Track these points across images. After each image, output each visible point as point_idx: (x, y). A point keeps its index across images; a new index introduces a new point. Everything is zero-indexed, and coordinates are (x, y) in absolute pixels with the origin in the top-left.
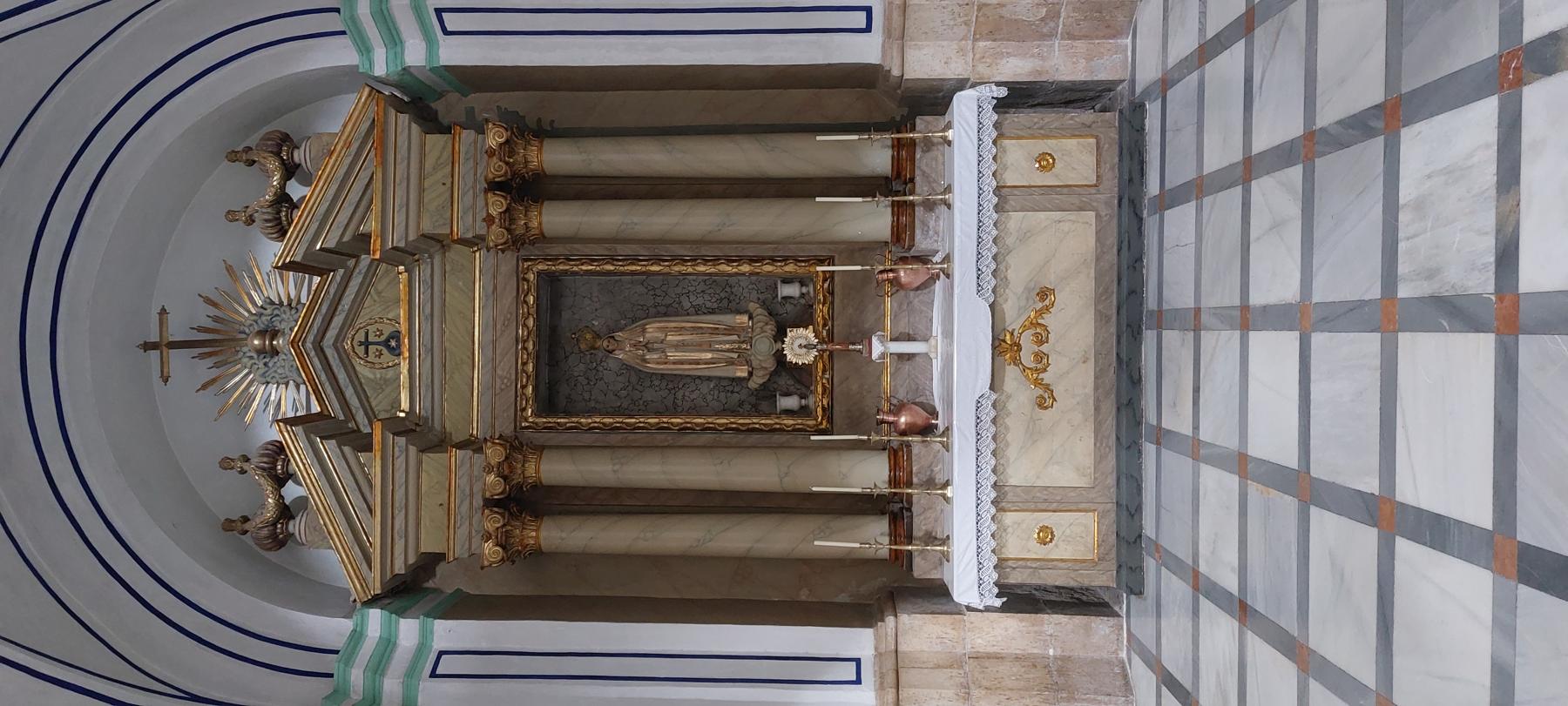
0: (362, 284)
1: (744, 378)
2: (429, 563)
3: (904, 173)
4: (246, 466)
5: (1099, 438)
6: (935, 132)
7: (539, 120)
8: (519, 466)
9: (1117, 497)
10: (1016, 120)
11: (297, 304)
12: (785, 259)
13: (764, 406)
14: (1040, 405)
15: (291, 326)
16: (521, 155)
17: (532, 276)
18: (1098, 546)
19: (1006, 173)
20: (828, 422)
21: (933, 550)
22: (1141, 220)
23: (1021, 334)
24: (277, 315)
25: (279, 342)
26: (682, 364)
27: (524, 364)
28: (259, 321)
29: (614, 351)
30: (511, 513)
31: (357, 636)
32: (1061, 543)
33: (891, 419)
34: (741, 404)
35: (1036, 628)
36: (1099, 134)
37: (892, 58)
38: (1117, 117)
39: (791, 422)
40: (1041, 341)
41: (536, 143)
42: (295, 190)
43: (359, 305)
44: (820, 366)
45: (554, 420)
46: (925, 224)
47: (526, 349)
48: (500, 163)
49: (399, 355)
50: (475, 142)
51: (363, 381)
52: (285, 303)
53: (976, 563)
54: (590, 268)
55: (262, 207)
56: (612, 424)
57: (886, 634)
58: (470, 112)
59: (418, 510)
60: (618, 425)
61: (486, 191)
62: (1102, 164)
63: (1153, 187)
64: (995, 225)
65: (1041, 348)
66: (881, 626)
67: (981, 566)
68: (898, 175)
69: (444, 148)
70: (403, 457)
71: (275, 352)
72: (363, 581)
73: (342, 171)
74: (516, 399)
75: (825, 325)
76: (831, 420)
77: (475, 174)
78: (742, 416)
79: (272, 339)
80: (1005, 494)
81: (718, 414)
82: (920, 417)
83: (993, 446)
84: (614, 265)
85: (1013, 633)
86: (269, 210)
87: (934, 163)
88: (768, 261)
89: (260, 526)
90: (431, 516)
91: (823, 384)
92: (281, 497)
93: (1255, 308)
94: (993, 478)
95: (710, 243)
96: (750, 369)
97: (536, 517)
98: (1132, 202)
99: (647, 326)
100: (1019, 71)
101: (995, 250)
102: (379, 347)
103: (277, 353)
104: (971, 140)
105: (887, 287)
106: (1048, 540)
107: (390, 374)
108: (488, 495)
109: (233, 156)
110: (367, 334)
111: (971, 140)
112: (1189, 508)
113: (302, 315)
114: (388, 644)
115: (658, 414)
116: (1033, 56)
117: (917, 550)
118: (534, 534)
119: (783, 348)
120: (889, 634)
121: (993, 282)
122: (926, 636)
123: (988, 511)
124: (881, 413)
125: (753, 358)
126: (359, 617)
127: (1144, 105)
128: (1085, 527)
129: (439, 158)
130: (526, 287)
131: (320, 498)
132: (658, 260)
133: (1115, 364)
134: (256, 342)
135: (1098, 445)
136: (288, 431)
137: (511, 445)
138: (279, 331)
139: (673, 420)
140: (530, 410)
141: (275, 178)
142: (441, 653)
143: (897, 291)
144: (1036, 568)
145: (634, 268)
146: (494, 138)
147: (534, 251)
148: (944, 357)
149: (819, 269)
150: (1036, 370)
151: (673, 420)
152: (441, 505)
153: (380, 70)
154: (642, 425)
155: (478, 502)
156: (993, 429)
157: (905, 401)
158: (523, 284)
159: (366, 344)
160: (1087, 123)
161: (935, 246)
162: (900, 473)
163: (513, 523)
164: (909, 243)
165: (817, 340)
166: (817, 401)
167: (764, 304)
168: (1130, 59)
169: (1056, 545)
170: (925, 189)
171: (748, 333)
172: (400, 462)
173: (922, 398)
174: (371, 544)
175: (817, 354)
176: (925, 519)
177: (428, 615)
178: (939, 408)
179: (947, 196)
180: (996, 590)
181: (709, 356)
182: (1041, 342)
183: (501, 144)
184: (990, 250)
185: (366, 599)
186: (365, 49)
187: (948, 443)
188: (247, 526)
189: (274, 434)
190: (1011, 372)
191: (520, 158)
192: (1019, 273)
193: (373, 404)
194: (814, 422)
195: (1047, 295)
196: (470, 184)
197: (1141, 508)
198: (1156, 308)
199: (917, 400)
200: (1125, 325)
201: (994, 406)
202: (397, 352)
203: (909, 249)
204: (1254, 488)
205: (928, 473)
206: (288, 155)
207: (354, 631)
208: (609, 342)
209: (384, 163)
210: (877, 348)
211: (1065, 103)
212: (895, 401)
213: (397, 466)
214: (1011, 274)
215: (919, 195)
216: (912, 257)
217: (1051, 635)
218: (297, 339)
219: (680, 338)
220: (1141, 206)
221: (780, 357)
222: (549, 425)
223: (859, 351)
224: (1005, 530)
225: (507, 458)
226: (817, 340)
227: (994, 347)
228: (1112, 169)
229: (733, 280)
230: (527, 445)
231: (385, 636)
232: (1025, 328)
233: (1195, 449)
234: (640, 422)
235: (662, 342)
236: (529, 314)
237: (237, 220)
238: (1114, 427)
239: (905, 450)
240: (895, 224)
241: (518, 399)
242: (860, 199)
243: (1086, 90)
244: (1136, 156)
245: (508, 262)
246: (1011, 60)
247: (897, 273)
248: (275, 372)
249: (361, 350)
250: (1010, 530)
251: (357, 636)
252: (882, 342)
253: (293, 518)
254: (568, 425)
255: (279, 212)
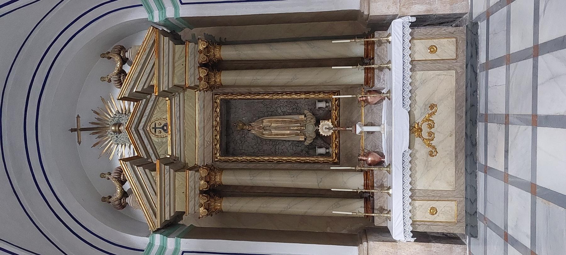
0: (153, 105)
1: (303, 141)
2: (179, 215)
3: (370, 55)
4: (109, 177)
5: (457, 169)
6: (383, 38)
7: (220, 38)
8: (213, 177)
9: (466, 195)
10: (419, 31)
11: (128, 113)
12: (319, 92)
13: (311, 152)
14: (430, 155)
15: (125, 121)
16: (212, 52)
17: (218, 101)
18: (457, 216)
19: (415, 55)
20: (338, 159)
21: (384, 216)
22: (476, 74)
23: (422, 124)
24: (121, 118)
25: (122, 128)
26: (278, 135)
27: (216, 136)
28: (114, 120)
29: (251, 130)
30: (211, 196)
31: (151, 245)
32: (440, 215)
33: (364, 158)
34: (302, 151)
35: (428, 249)
36: (457, 37)
37: (365, 7)
38: (465, 29)
39: (322, 159)
40: (431, 127)
41: (219, 48)
42: (127, 68)
43: (152, 113)
44: (334, 136)
45: (228, 158)
46: (379, 77)
47: (216, 130)
48: (204, 56)
49: (167, 133)
50: (195, 47)
51: (154, 143)
52: (124, 113)
53: (403, 223)
54: (241, 97)
55: (114, 75)
56: (250, 159)
57: (363, 249)
58: (194, 36)
59: (174, 194)
60: (253, 160)
61: (199, 67)
62: (459, 50)
63: (482, 59)
64: (410, 77)
65: (431, 130)
66: (361, 246)
67: (405, 224)
68: (367, 57)
69: (182, 50)
70: (168, 174)
71: (120, 132)
72: (153, 223)
73: (143, 61)
74: (213, 150)
75: (336, 119)
76: (339, 159)
77: (195, 60)
78: (303, 157)
79: (119, 127)
80: (415, 193)
81: (292, 155)
82: (377, 158)
83: (410, 173)
84: (250, 96)
85: (419, 251)
86: (116, 76)
87: (383, 51)
88: (312, 93)
89: (115, 200)
90: (180, 197)
91: (335, 143)
92: (123, 189)
93: (540, 116)
94: (410, 187)
95: (286, 86)
96: (305, 137)
97: (220, 197)
98: (472, 66)
99: (264, 120)
100: (420, 10)
101: (410, 88)
102: (160, 130)
103: (121, 133)
104: (399, 40)
105: (363, 103)
106: (435, 213)
107: (164, 140)
108: (201, 189)
109: (103, 56)
110: (155, 124)
111: (399, 40)
112: (502, 204)
113: (130, 118)
114: (163, 248)
115: (268, 155)
116: (426, 4)
117: (377, 216)
118: (219, 204)
119: (319, 129)
120: (365, 249)
121: (410, 102)
122: (380, 251)
123: (408, 201)
124: (360, 156)
125: (306, 133)
126: (152, 237)
127: (478, 23)
128: (451, 208)
129: (180, 55)
130: (216, 105)
131: (137, 190)
132: (268, 94)
133: (464, 137)
134: (113, 128)
135: (457, 172)
136: (124, 164)
137: (210, 169)
138: (122, 124)
139: (274, 158)
140: (218, 154)
141: (118, 64)
142: (183, 252)
143: (367, 105)
144: (429, 225)
145: (258, 97)
146: (202, 46)
147: (219, 91)
148: (388, 134)
149: (333, 97)
150: (429, 140)
151: (274, 158)
152: (183, 192)
153: (156, 20)
154: (262, 160)
155: (197, 192)
156: (410, 166)
157: (370, 150)
158: (215, 104)
159: (155, 128)
160: (451, 32)
161: (383, 86)
162: (369, 185)
163: (211, 200)
164: (372, 85)
165: (333, 126)
166: (333, 150)
167: (310, 110)
168: (470, 4)
169: (438, 215)
170: (379, 62)
171: (304, 122)
172: (167, 176)
173: (378, 149)
174: (156, 207)
175: (333, 131)
176: (379, 201)
177: (178, 237)
178: (385, 154)
179: (389, 65)
180: (412, 235)
181: (289, 132)
182: (431, 128)
183: (204, 48)
184: (408, 88)
185: (154, 230)
186: (150, 11)
187: (390, 171)
188: (110, 200)
189: (118, 164)
190: (418, 141)
191: (212, 53)
192: (421, 98)
193: (158, 152)
194: (332, 159)
195: (433, 107)
196: (193, 64)
197: (477, 200)
198: (484, 113)
199: (375, 150)
200: (469, 120)
201: (410, 155)
202: (167, 131)
203: (372, 87)
204: (539, 201)
205: (381, 182)
206: (123, 55)
207: (150, 243)
208: (249, 127)
209: (159, 57)
210: (358, 130)
211: (439, 24)
212: (366, 151)
213: (166, 177)
214: (417, 98)
215: (377, 65)
216: (373, 90)
217: (435, 252)
218: (128, 127)
219: (277, 125)
220: (477, 67)
221: (317, 132)
222: (226, 160)
223: (351, 130)
224: (415, 209)
225: (208, 174)
226: (333, 126)
227: (410, 130)
228: (463, 51)
229: (298, 101)
230: (217, 169)
231: (162, 245)
232: (424, 121)
233: (506, 178)
234: (261, 159)
235: (270, 127)
236: (217, 116)
237: (105, 81)
238: (464, 164)
239: (371, 172)
240: (366, 77)
241: (214, 150)
242: (351, 67)
243: (449, 18)
244: (474, 46)
245: (209, 95)
246: (417, 6)
247: (367, 97)
248: (121, 140)
249: (153, 131)
250: (417, 208)
251: (151, 245)
252: (360, 127)
253: (128, 197)
254: (233, 160)
255: (120, 77)
